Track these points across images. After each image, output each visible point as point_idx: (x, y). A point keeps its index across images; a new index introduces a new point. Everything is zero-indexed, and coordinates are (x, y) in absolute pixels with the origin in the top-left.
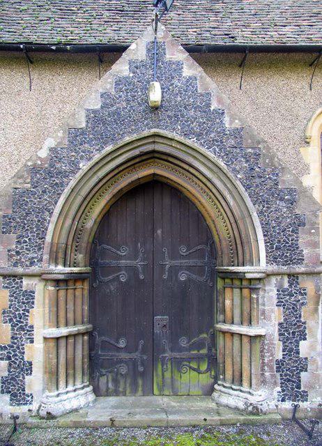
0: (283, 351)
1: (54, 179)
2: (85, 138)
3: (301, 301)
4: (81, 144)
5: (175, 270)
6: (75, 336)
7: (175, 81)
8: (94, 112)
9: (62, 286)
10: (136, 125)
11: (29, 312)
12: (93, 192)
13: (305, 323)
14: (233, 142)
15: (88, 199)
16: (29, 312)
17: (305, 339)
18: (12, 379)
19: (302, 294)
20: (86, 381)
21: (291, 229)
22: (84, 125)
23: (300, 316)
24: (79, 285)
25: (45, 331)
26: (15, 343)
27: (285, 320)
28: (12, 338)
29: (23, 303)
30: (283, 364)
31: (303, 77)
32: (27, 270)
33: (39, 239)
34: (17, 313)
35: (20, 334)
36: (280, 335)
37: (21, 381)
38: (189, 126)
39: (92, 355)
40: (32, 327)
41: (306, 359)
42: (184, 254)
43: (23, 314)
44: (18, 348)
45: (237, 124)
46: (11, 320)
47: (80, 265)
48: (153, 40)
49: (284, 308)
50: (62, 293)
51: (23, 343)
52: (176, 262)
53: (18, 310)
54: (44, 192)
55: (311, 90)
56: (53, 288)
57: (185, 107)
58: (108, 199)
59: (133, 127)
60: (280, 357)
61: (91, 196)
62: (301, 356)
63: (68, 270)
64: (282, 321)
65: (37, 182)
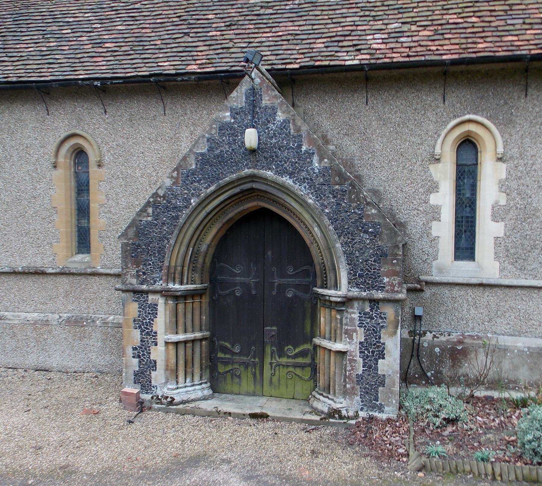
0: (363, 367)
1: (170, 213)
2: (195, 178)
3: (382, 324)
4: (192, 183)
5: (282, 288)
6: (193, 341)
7: (271, 126)
8: (202, 155)
9: (182, 301)
10: (237, 165)
11: (153, 321)
12: (204, 223)
13: (384, 344)
14: (322, 180)
15: (200, 228)
16: (153, 321)
17: (383, 358)
18: (142, 373)
19: (382, 318)
20: (204, 378)
21: (373, 259)
22: (194, 167)
23: (380, 338)
24: (197, 300)
25: (166, 337)
26: (143, 345)
27: (366, 340)
28: (141, 341)
29: (149, 313)
30: (362, 378)
31: (436, 88)
32: (150, 288)
33: (160, 262)
34: (144, 321)
35: (147, 338)
36: (360, 352)
37: (149, 375)
38: (282, 166)
39: (212, 358)
40: (156, 333)
41: (384, 375)
42: (291, 274)
43: (149, 322)
44: (146, 349)
45: (326, 163)
46: (140, 327)
47: (197, 282)
48: (250, 87)
49: (365, 329)
50: (181, 307)
51: (149, 345)
52: (284, 281)
53: (145, 319)
54: (163, 224)
55: (444, 101)
56: (172, 302)
57: (279, 149)
58: (219, 228)
59: (235, 168)
60: (360, 372)
61: (202, 226)
62: (379, 372)
63: (183, 287)
64: (363, 340)
65: (157, 216)
